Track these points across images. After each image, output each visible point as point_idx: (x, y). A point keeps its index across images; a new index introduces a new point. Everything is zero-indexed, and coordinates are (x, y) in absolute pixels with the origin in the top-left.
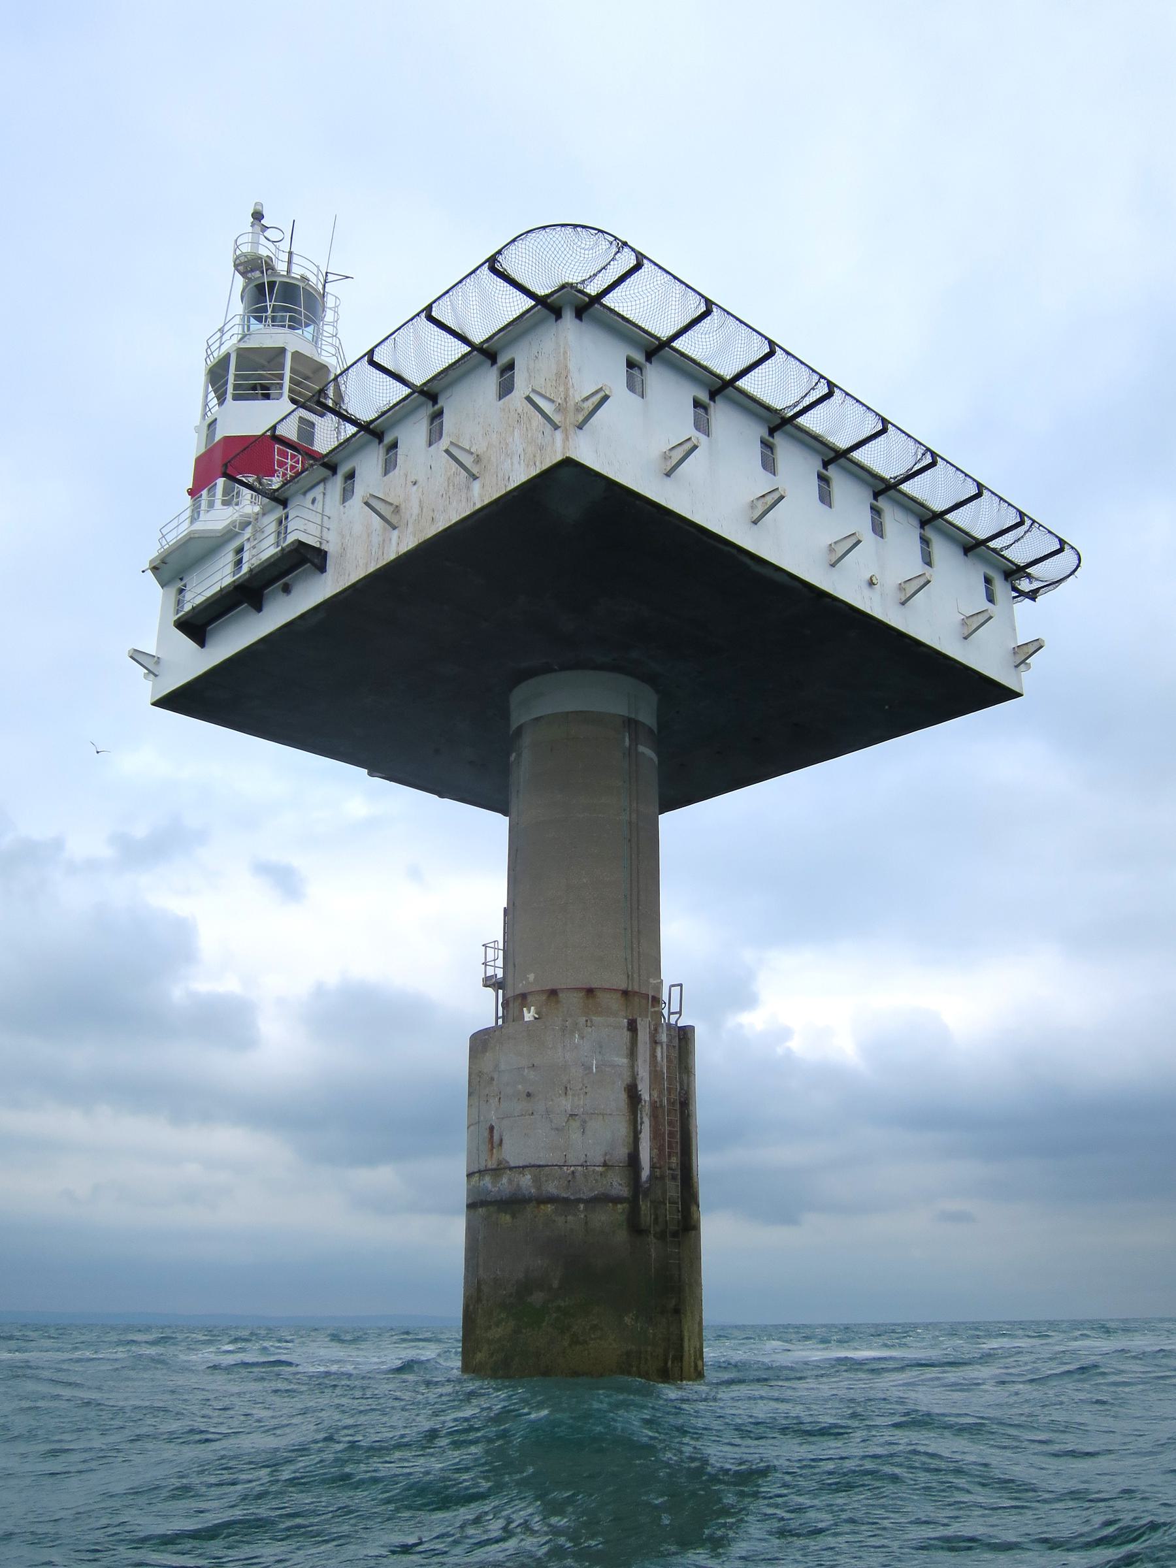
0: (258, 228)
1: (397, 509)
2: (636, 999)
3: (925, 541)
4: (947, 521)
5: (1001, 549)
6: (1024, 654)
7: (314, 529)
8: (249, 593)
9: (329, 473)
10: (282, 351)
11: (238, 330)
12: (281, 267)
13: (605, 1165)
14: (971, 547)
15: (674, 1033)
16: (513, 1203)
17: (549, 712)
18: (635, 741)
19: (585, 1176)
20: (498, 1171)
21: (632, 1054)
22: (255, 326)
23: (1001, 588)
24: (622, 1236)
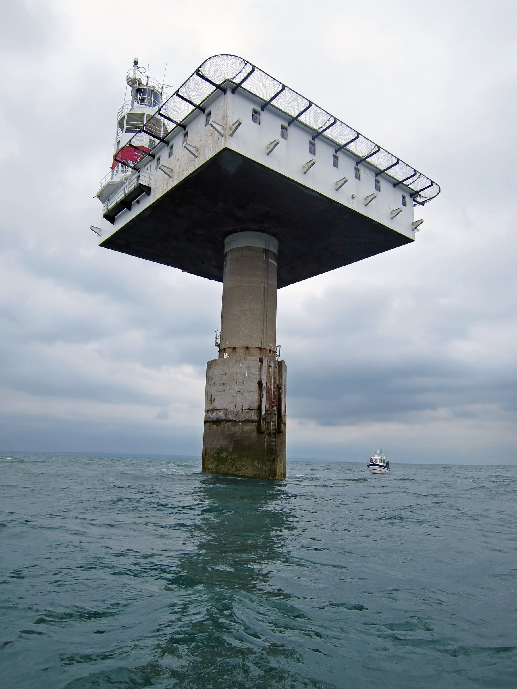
0: (136, 68)
1: (172, 170)
2: (265, 351)
3: (377, 182)
4: (386, 174)
5: (409, 185)
6: (416, 225)
7: (147, 180)
8: (126, 204)
9: (152, 158)
10: (144, 114)
11: (130, 107)
12: (144, 82)
13: (249, 409)
14: (397, 184)
15: (277, 363)
16: (217, 422)
17: (237, 247)
18: (267, 257)
19: (242, 413)
20: (213, 410)
21: (261, 370)
22: (136, 105)
23: (408, 199)
24: (255, 434)
